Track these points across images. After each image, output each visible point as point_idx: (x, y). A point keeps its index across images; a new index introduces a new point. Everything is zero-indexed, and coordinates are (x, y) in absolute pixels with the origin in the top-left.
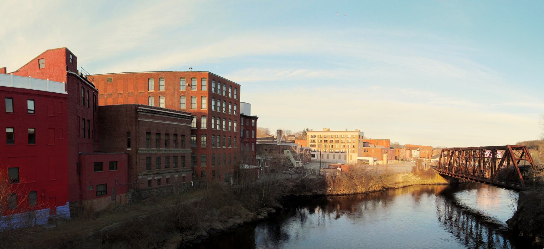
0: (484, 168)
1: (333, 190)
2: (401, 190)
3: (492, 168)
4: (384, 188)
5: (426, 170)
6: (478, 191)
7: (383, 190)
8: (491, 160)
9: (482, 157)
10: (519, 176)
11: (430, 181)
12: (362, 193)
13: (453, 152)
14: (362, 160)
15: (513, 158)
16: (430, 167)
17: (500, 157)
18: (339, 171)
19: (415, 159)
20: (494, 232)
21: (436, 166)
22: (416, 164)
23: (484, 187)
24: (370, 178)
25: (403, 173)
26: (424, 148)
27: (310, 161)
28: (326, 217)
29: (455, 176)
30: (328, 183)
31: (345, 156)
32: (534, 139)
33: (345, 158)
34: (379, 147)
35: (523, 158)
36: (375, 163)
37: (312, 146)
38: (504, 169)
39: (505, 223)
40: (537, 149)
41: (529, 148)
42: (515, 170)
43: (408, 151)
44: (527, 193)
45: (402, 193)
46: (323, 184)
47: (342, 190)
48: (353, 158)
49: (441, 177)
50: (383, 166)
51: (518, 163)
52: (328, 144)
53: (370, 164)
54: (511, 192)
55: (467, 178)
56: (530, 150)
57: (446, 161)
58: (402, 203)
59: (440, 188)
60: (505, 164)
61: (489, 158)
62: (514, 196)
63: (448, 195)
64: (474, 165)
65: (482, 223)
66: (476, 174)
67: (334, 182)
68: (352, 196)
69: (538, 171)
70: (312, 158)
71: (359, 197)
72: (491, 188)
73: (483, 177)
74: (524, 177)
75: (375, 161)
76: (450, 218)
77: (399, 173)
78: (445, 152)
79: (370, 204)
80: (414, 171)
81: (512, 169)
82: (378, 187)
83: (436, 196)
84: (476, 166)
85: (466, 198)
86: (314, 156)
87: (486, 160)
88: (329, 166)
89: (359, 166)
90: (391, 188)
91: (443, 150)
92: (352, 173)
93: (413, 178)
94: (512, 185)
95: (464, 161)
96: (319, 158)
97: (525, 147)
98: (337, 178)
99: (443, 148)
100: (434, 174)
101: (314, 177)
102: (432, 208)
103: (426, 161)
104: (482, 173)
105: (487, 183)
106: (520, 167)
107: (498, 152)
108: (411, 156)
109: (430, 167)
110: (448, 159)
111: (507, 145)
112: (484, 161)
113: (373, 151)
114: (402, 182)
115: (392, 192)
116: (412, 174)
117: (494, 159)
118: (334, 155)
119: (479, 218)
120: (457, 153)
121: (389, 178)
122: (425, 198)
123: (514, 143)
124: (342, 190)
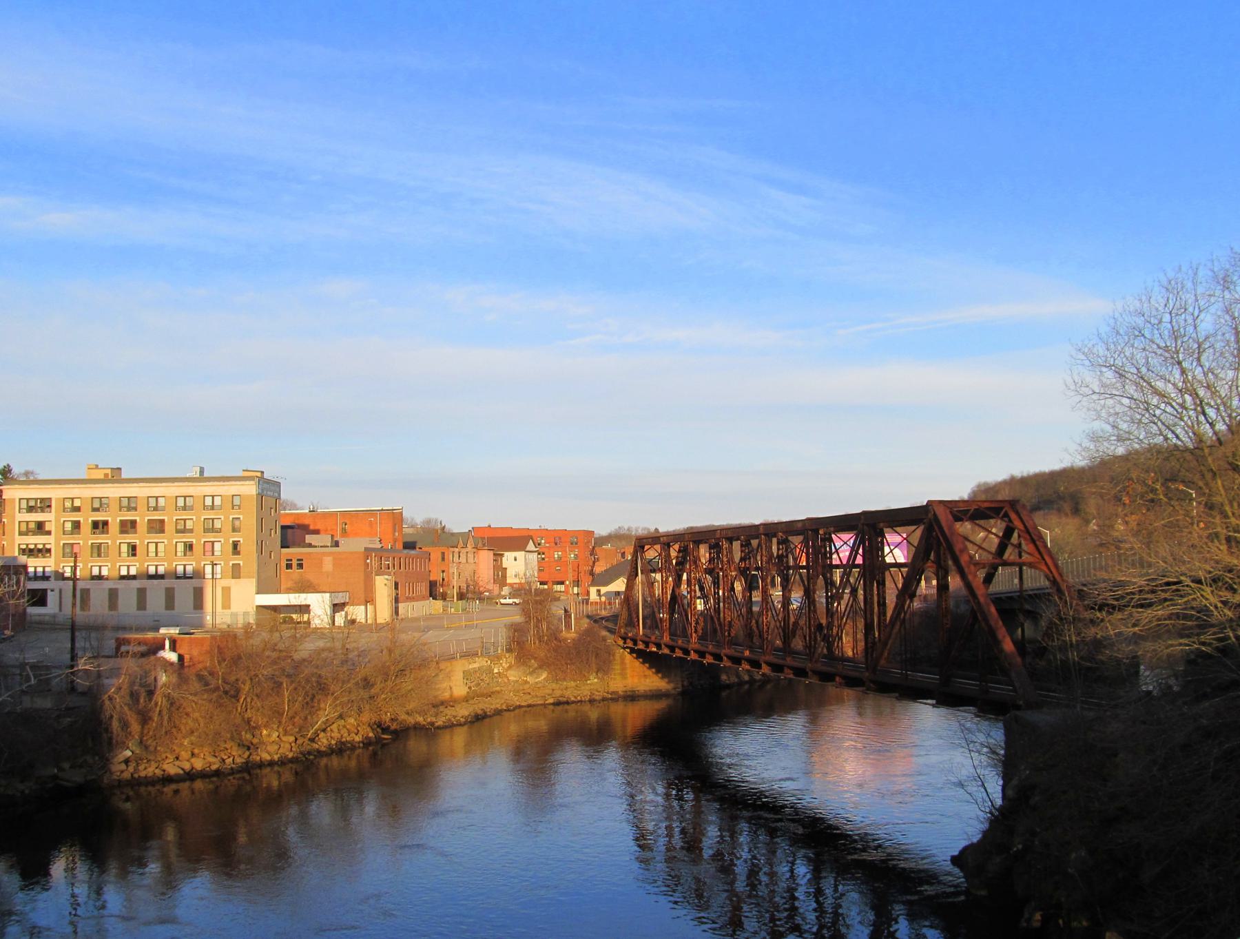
0: (830, 613)
1: (138, 760)
2: (459, 738)
3: (869, 612)
4: (386, 730)
5: (570, 635)
6: (814, 720)
7: (378, 740)
8: (863, 575)
9: (821, 561)
10: (997, 642)
11: (593, 685)
12: (283, 762)
13: (684, 551)
14: (275, 609)
15: (964, 559)
16: (585, 623)
17: (901, 560)
18: (167, 664)
19: (517, 591)
20: (898, 909)
21: (614, 618)
22: (526, 613)
23: (840, 700)
24: (316, 689)
25: (472, 662)
26: (558, 538)
27: (22, 623)
28: (113, 897)
29: (702, 654)
30: (115, 724)
31: (199, 594)
32: (1057, 466)
33: (198, 603)
34: (354, 545)
35: (1010, 554)
36: (340, 619)
37: (31, 552)
38: (925, 614)
39: (949, 867)
40: (1076, 511)
41: (1036, 508)
42: (976, 614)
43: (486, 557)
44: (1042, 718)
45: (468, 747)
46: (87, 727)
47: (185, 755)
48: (236, 602)
49: (637, 663)
50: (378, 628)
51: (989, 579)
52: (113, 539)
53: (316, 623)
54: (967, 717)
55: (755, 664)
56: (1038, 518)
57: (658, 592)
58: (476, 793)
59: (636, 716)
60: (927, 587)
61: (848, 567)
62: (981, 738)
63: (676, 742)
64: (786, 601)
65: (844, 870)
66: (798, 644)
67: (145, 719)
68: (232, 783)
69: (1087, 615)
70: (34, 611)
71: (272, 780)
72: (870, 702)
73: (831, 657)
74: (1020, 645)
75: (337, 607)
76: (692, 845)
77: (452, 658)
78: (652, 553)
79: (322, 810)
80: (518, 644)
81: (963, 608)
82: (353, 728)
83: (625, 746)
84: (795, 605)
85: (761, 755)
86: (39, 598)
87: (837, 575)
88: (120, 642)
89: (265, 635)
90: (417, 728)
91: (641, 544)
92: (244, 670)
93: (513, 676)
94: (930, 678)
95: (738, 587)
96: (67, 609)
97: (1013, 504)
98: (158, 698)
99: (640, 532)
100: (610, 653)
101: (45, 703)
102: (604, 807)
103: (567, 593)
104: (826, 638)
105: (852, 682)
106: (998, 600)
107: (891, 537)
108: (500, 575)
109: (585, 623)
110: (664, 582)
111: (930, 503)
112: (829, 583)
113: (328, 564)
114: (466, 699)
115: (423, 747)
116: (507, 660)
117: (874, 568)
118: (142, 593)
119: (824, 840)
120: (704, 553)
121: (407, 684)
122: (572, 763)
123: (958, 490)
124: (189, 751)
